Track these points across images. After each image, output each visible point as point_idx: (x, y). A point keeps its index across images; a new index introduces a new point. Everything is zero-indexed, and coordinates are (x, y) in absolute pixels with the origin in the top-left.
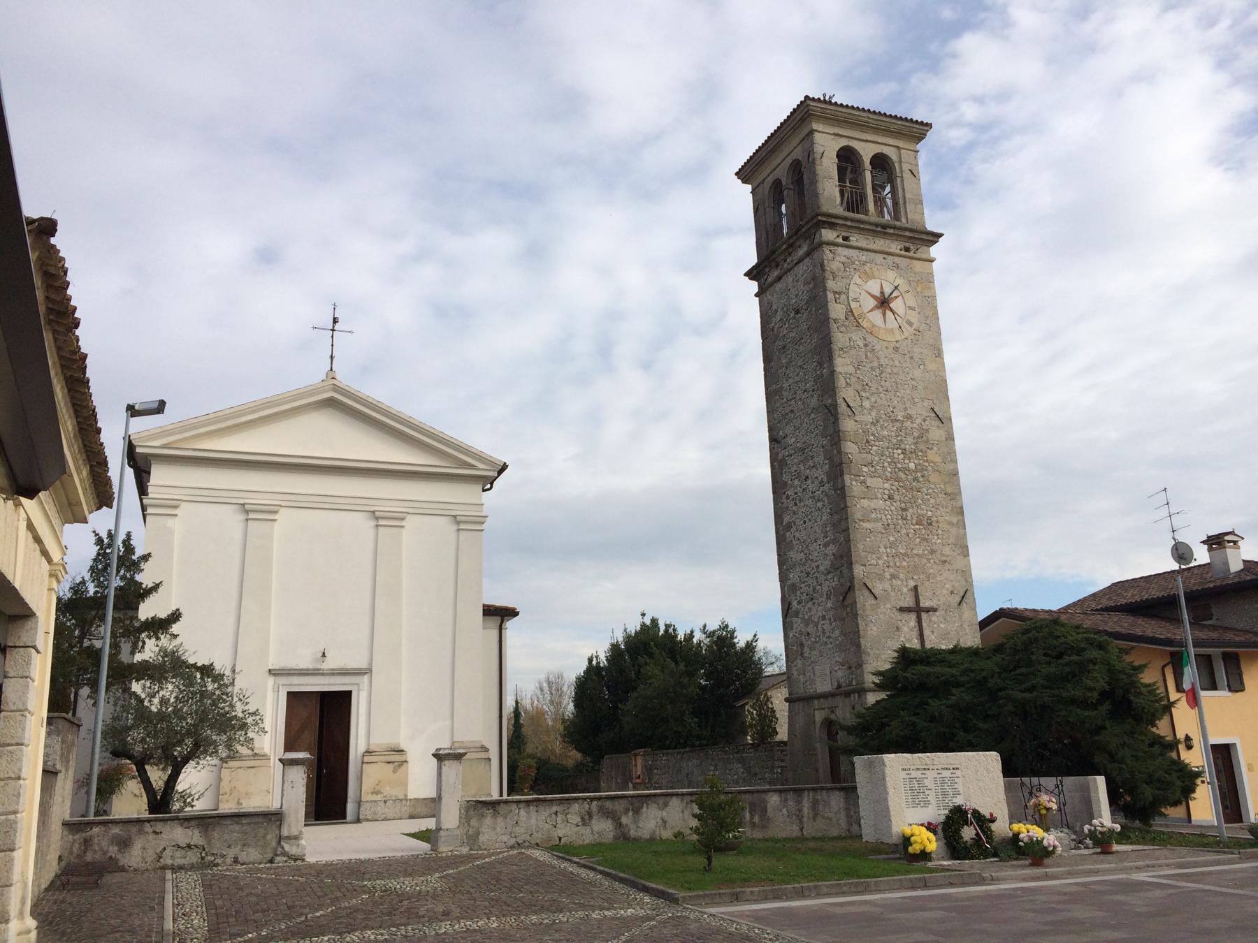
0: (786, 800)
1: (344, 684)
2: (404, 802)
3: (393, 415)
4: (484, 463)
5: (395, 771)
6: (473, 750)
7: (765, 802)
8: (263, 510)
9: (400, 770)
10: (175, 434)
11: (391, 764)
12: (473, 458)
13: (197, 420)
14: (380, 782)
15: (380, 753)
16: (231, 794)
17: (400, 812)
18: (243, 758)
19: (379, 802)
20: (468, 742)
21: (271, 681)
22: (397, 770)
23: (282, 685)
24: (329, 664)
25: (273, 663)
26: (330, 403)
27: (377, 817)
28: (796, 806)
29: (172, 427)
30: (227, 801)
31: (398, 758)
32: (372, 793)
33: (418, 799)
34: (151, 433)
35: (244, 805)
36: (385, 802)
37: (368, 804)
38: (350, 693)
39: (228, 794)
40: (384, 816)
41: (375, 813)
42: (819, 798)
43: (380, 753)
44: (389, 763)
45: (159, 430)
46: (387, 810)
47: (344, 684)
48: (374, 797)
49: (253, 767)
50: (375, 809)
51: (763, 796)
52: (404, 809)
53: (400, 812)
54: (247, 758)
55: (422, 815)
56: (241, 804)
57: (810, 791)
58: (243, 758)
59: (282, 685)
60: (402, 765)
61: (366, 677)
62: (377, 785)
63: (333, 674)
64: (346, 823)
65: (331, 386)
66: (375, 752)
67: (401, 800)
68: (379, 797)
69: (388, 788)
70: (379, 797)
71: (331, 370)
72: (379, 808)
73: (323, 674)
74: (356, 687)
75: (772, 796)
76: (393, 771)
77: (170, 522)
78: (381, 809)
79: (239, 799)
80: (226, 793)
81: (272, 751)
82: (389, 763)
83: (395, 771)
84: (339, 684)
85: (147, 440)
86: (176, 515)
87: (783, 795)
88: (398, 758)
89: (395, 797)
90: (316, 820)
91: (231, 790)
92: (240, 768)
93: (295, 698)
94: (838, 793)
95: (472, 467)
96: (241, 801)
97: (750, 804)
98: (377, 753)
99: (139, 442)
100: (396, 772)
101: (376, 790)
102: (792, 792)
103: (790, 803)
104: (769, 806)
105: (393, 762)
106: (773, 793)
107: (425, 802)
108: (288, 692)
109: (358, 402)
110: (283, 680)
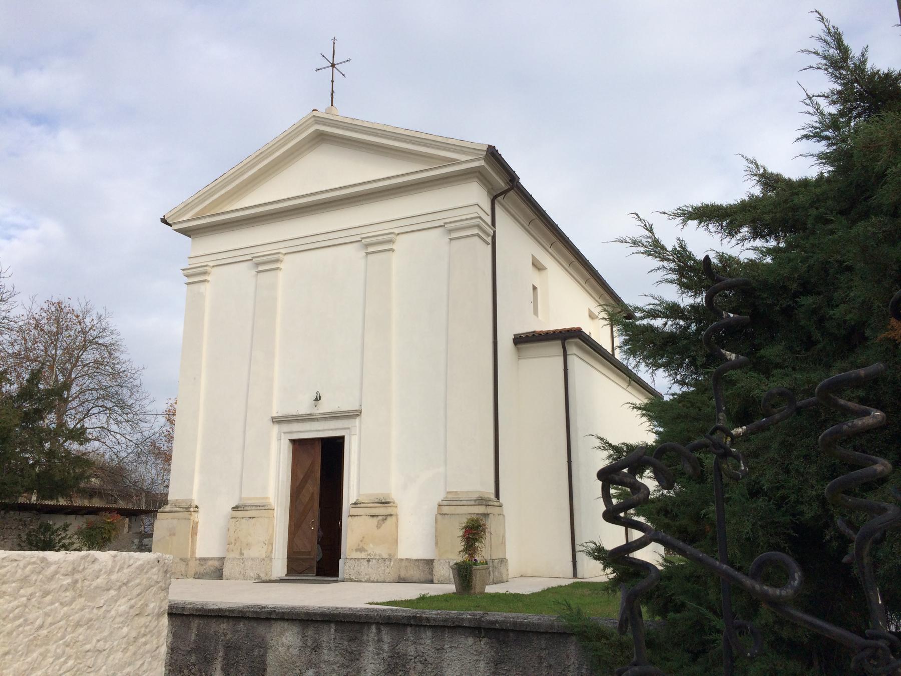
0: (317, 648)
1: (336, 429)
2: (387, 562)
4: (467, 153)
5: (378, 527)
6: (465, 502)
7: (264, 646)
8: (269, 260)
10: (197, 205)
11: (375, 518)
14: (364, 537)
17: (384, 574)
19: (362, 561)
20: (462, 492)
21: (276, 429)
22: (381, 525)
23: (284, 433)
24: (326, 407)
25: (277, 410)
26: (320, 139)
28: (343, 666)
30: (232, 551)
31: (382, 511)
32: (357, 550)
33: (410, 560)
34: (178, 209)
35: (245, 555)
36: (369, 561)
38: (342, 438)
39: (234, 544)
41: (359, 573)
42: (411, 650)
44: (373, 516)
46: (370, 570)
47: (336, 429)
51: (261, 629)
52: (388, 570)
53: (384, 574)
55: (414, 579)
59: (284, 433)
60: (386, 519)
61: (358, 419)
62: (361, 541)
64: (337, 581)
65: (313, 119)
66: (363, 503)
67: (384, 560)
68: (363, 555)
69: (371, 545)
70: (363, 555)
72: (363, 568)
73: (317, 419)
74: (348, 431)
78: (365, 570)
79: (241, 549)
81: (276, 503)
82: (373, 516)
83: (378, 527)
84: (332, 430)
85: (180, 216)
86: (205, 281)
87: (310, 632)
88: (382, 511)
90: (317, 575)
91: (235, 540)
92: (243, 518)
93: (299, 445)
94: (470, 641)
96: (243, 552)
99: (172, 220)
100: (379, 528)
101: (360, 547)
102: (333, 627)
104: (271, 658)
105: (377, 516)
106: (286, 625)
108: (294, 442)
109: (427, 145)
110: (286, 427)
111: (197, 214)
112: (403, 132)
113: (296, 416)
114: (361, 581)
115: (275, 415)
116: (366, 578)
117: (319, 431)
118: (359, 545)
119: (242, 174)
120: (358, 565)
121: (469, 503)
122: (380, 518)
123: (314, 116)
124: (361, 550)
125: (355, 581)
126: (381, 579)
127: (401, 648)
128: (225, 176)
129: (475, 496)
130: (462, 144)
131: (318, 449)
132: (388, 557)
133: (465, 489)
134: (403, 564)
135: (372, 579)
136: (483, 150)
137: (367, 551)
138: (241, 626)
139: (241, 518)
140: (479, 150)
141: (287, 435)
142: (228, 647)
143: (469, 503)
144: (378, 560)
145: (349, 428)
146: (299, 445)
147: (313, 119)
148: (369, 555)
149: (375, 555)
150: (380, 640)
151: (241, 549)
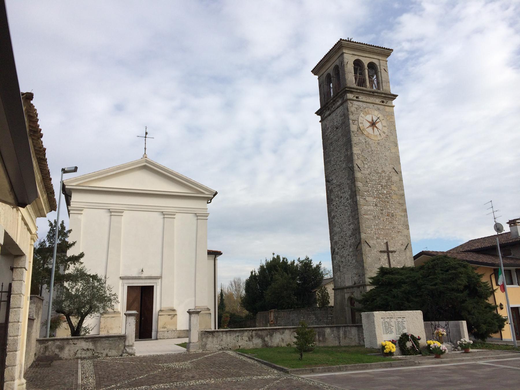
0: (333, 331)
2: (175, 331)
4: (207, 191)
5: (171, 319)
7: (325, 332)
10: (81, 180)
11: (170, 316)
17: (174, 335)
23: (126, 283)
24: (145, 275)
25: (122, 274)
27: (164, 338)
29: (80, 177)
30: (103, 331)
32: (162, 328)
36: (168, 331)
37: (161, 332)
38: (153, 287)
40: (167, 337)
44: (169, 315)
49: (114, 317)
51: (323, 329)
52: (176, 334)
56: (109, 332)
58: (110, 313)
59: (126, 283)
60: (174, 316)
61: (160, 280)
62: (164, 324)
64: (152, 340)
65: (145, 161)
67: (174, 331)
68: (165, 330)
69: (169, 326)
70: (165, 330)
71: (145, 154)
72: (165, 334)
73: (142, 279)
74: (156, 284)
78: (166, 334)
82: (169, 315)
83: (171, 319)
87: (332, 329)
92: (108, 317)
93: (130, 288)
94: (355, 328)
96: (109, 331)
98: (164, 311)
105: (171, 315)
106: (328, 328)
107: (184, 331)
108: (128, 286)
111: (80, 184)
112: (185, 177)
113: (131, 277)
114: (165, 339)
115: (121, 276)
116: (167, 337)
117: (142, 283)
118: (163, 326)
119: (107, 173)
120: (163, 333)
121: (205, 310)
122: (172, 315)
123: (146, 160)
124: (164, 328)
125: (162, 339)
126: (172, 337)
127: (346, 330)
128: (99, 172)
129: (206, 308)
130: (207, 188)
131: (139, 292)
132: (175, 330)
133: (203, 305)
134: (179, 331)
135: (169, 338)
136: (214, 192)
137: (167, 328)
138: (320, 329)
139: (107, 317)
140: (213, 192)
141: (127, 284)
142: (318, 332)
143: (205, 310)
144: (172, 331)
145: (156, 283)
146: (130, 288)
147: (145, 161)
148: (168, 329)
149: (170, 329)
150: (343, 329)
151: (108, 330)
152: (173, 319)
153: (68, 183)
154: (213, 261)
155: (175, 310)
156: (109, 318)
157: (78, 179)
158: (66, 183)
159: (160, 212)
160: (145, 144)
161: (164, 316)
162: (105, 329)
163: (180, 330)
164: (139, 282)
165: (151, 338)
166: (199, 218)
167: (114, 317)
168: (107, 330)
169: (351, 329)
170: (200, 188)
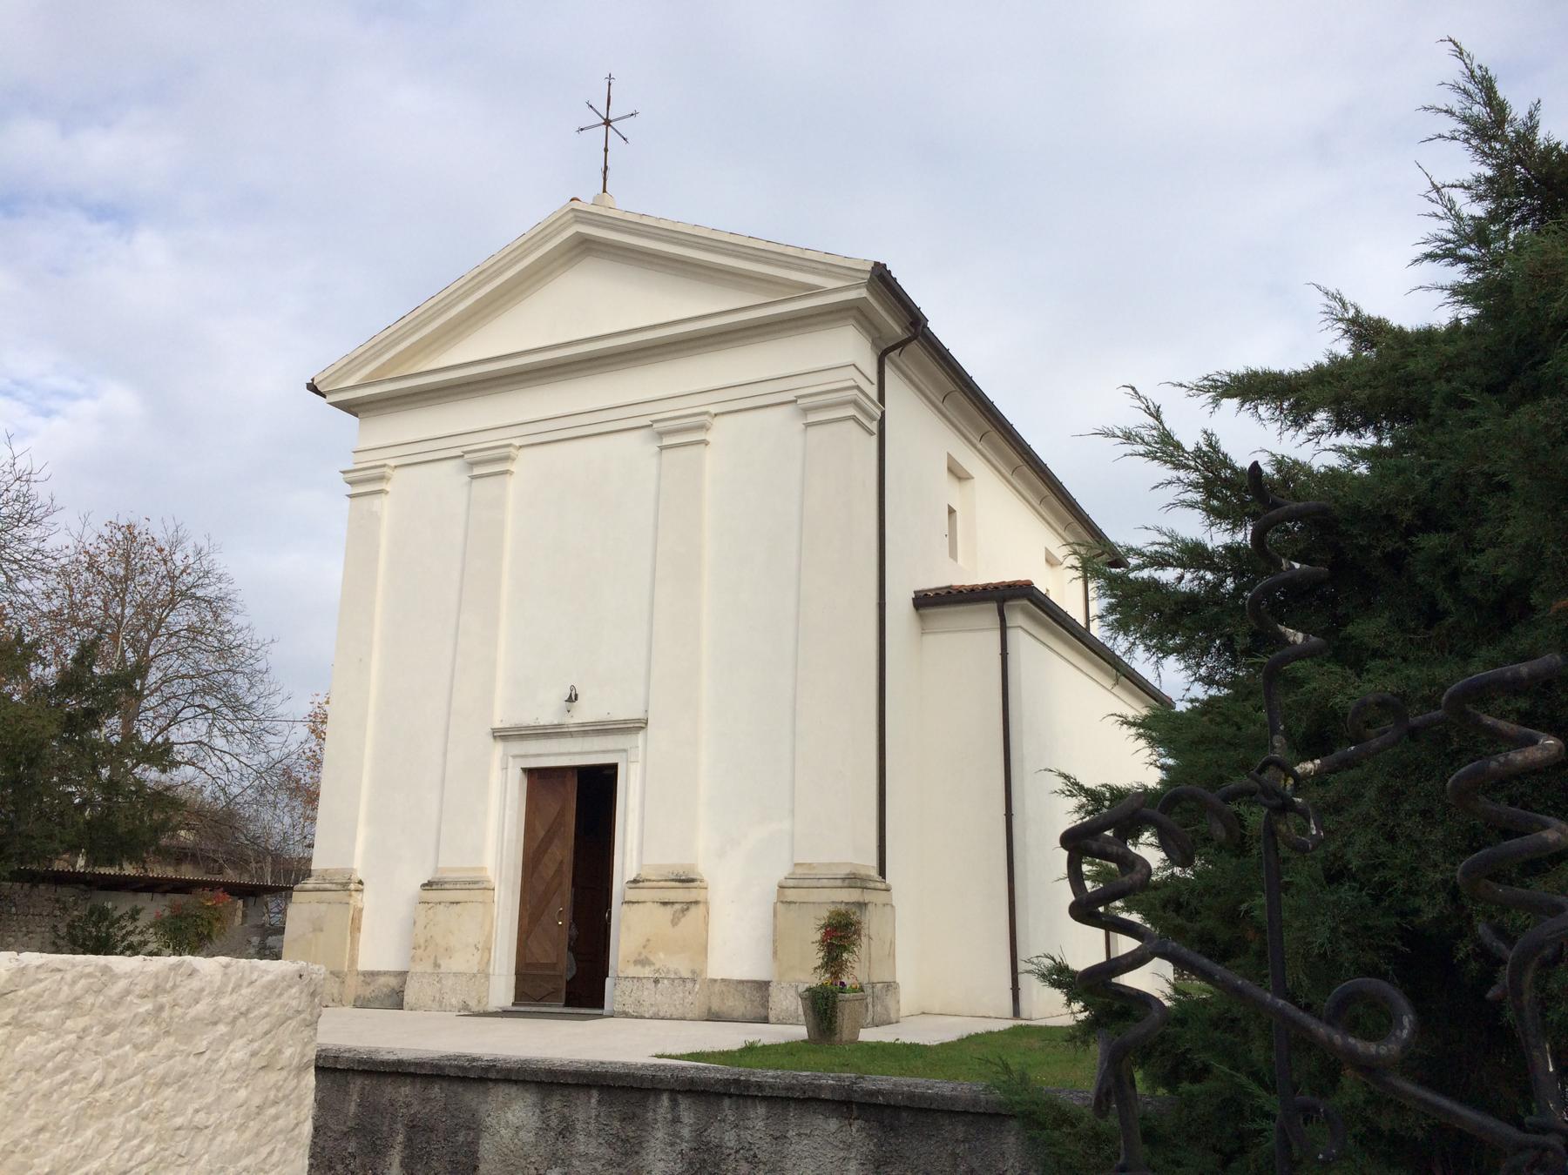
0: (566, 1131)
2: (689, 985)
3: (731, 247)
4: (837, 276)
5: (674, 923)
7: (474, 1127)
9: (683, 920)
10: (368, 362)
12: (814, 271)
13: (390, 331)
14: (648, 940)
15: (654, 884)
16: (426, 947)
18: (447, 886)
21: (499, 748)
22: (679, 919)
23: (514, 757)
24: (586, 713)
25: (502, 717)
26: (584, 248)
27: (642, 1010)
29: (361, 350)
32: (636, 962)
35: (442, 967)
36: (656, 981)
37: (626, 983)
40: (654, 1009)
42: (730, 1139)
43: (654, 884)
44: (665, 904)
45: (346, 361)
46: (659, 997)
48: (634, 971)
49: (457, 903)
50: (639, 993)
51: (470, 1097)
54: (451, 886)
55: (736, 1014)
56: (439, 966)
57: (684, 1103)
58: (447, 886)
60: (688, 909)
61: (641, 735)
62: (644, 947)
63: (585, 733)
64: (601, 1016)
65: (571, 215)
66: (648, 880)
67: (684, 980)
68: (646, 972)
69: (662, 955)
70: (646, 972)
71: (604, 191)
72: (646, 993)
73: (571, 734)
74: (624, 755)
75: (506, 1105)
76: (672, 921)
77: (377, 502)
78: (650, 997)
80: (420, 947)
82: (665, 904)
83: (674, 923)
84: (596, 752)
85: (335, 381)
87: (555, 1104)
89: (676, 973)
90: (567, 1005)
91: (426, 941)
92: (440, 903)
93: (538, 778)
94: (833, 1124)
95: (813, 291)
96: (440, 961)
97: (414, 1127)
98: (646, 884)
99: (327, 387)
101: (643, 957)
103: (583, 1144)
104: (486, 1148)
105: (673, 903)
106: (513, 1090)
107: (740, 987)
113: (535, 728)
114: (642, 1017)
115: (498, 725)
118: (640, 954)
121: (832, 883)
122: (677, 907)
124: (642, 962)
127: (713, 1134)
129: (843, 872)
131: (571, 786)
135: (661, 1014)
136: (864, 271)
137: (654, 964)
138: (436, 1091)
139: (436, 903)
142: (413, 1127)
143: (832, 883)
145: (625, 751)
147: (571, 215)
148: (658, 971)
149: (668, 971)
150: (676, 1120)
152: (680, 924)
153: (330, 384)
154: (997, 635)
155: (693, 880)
156: (442, 906)
157: (356, 358)
158: (324, 383)
159: (642, 432)
160: (606, 150)
161: (641, 905)
162: (429, 949)
163: (722, 980)
164: (562, 750)
165: (602, 1007)
166: (812, 418)
167: (457, 903)
168: (433, 958)
169: (780, 1138)
170: (801, 269)
